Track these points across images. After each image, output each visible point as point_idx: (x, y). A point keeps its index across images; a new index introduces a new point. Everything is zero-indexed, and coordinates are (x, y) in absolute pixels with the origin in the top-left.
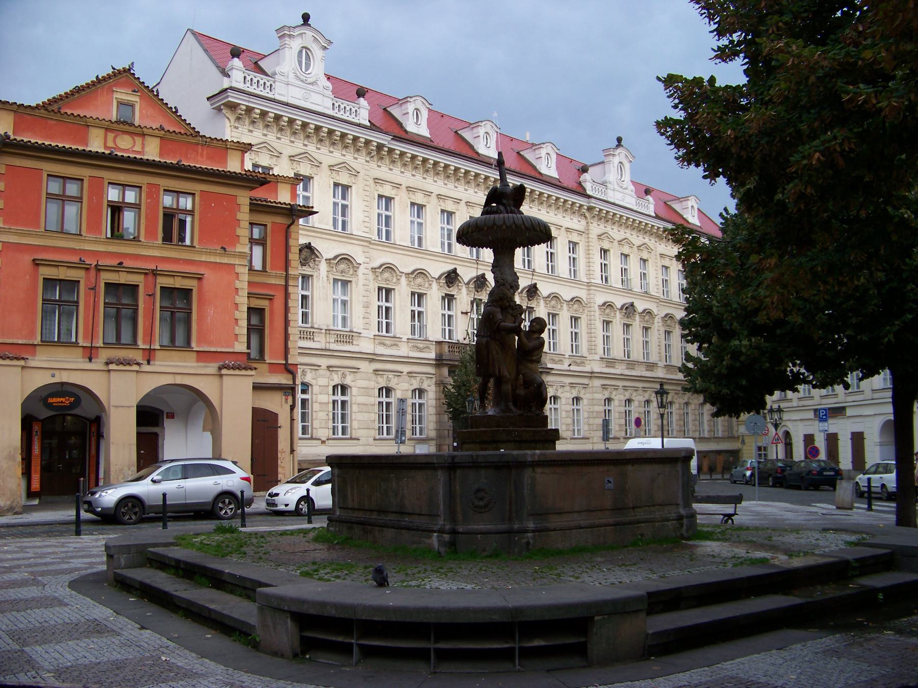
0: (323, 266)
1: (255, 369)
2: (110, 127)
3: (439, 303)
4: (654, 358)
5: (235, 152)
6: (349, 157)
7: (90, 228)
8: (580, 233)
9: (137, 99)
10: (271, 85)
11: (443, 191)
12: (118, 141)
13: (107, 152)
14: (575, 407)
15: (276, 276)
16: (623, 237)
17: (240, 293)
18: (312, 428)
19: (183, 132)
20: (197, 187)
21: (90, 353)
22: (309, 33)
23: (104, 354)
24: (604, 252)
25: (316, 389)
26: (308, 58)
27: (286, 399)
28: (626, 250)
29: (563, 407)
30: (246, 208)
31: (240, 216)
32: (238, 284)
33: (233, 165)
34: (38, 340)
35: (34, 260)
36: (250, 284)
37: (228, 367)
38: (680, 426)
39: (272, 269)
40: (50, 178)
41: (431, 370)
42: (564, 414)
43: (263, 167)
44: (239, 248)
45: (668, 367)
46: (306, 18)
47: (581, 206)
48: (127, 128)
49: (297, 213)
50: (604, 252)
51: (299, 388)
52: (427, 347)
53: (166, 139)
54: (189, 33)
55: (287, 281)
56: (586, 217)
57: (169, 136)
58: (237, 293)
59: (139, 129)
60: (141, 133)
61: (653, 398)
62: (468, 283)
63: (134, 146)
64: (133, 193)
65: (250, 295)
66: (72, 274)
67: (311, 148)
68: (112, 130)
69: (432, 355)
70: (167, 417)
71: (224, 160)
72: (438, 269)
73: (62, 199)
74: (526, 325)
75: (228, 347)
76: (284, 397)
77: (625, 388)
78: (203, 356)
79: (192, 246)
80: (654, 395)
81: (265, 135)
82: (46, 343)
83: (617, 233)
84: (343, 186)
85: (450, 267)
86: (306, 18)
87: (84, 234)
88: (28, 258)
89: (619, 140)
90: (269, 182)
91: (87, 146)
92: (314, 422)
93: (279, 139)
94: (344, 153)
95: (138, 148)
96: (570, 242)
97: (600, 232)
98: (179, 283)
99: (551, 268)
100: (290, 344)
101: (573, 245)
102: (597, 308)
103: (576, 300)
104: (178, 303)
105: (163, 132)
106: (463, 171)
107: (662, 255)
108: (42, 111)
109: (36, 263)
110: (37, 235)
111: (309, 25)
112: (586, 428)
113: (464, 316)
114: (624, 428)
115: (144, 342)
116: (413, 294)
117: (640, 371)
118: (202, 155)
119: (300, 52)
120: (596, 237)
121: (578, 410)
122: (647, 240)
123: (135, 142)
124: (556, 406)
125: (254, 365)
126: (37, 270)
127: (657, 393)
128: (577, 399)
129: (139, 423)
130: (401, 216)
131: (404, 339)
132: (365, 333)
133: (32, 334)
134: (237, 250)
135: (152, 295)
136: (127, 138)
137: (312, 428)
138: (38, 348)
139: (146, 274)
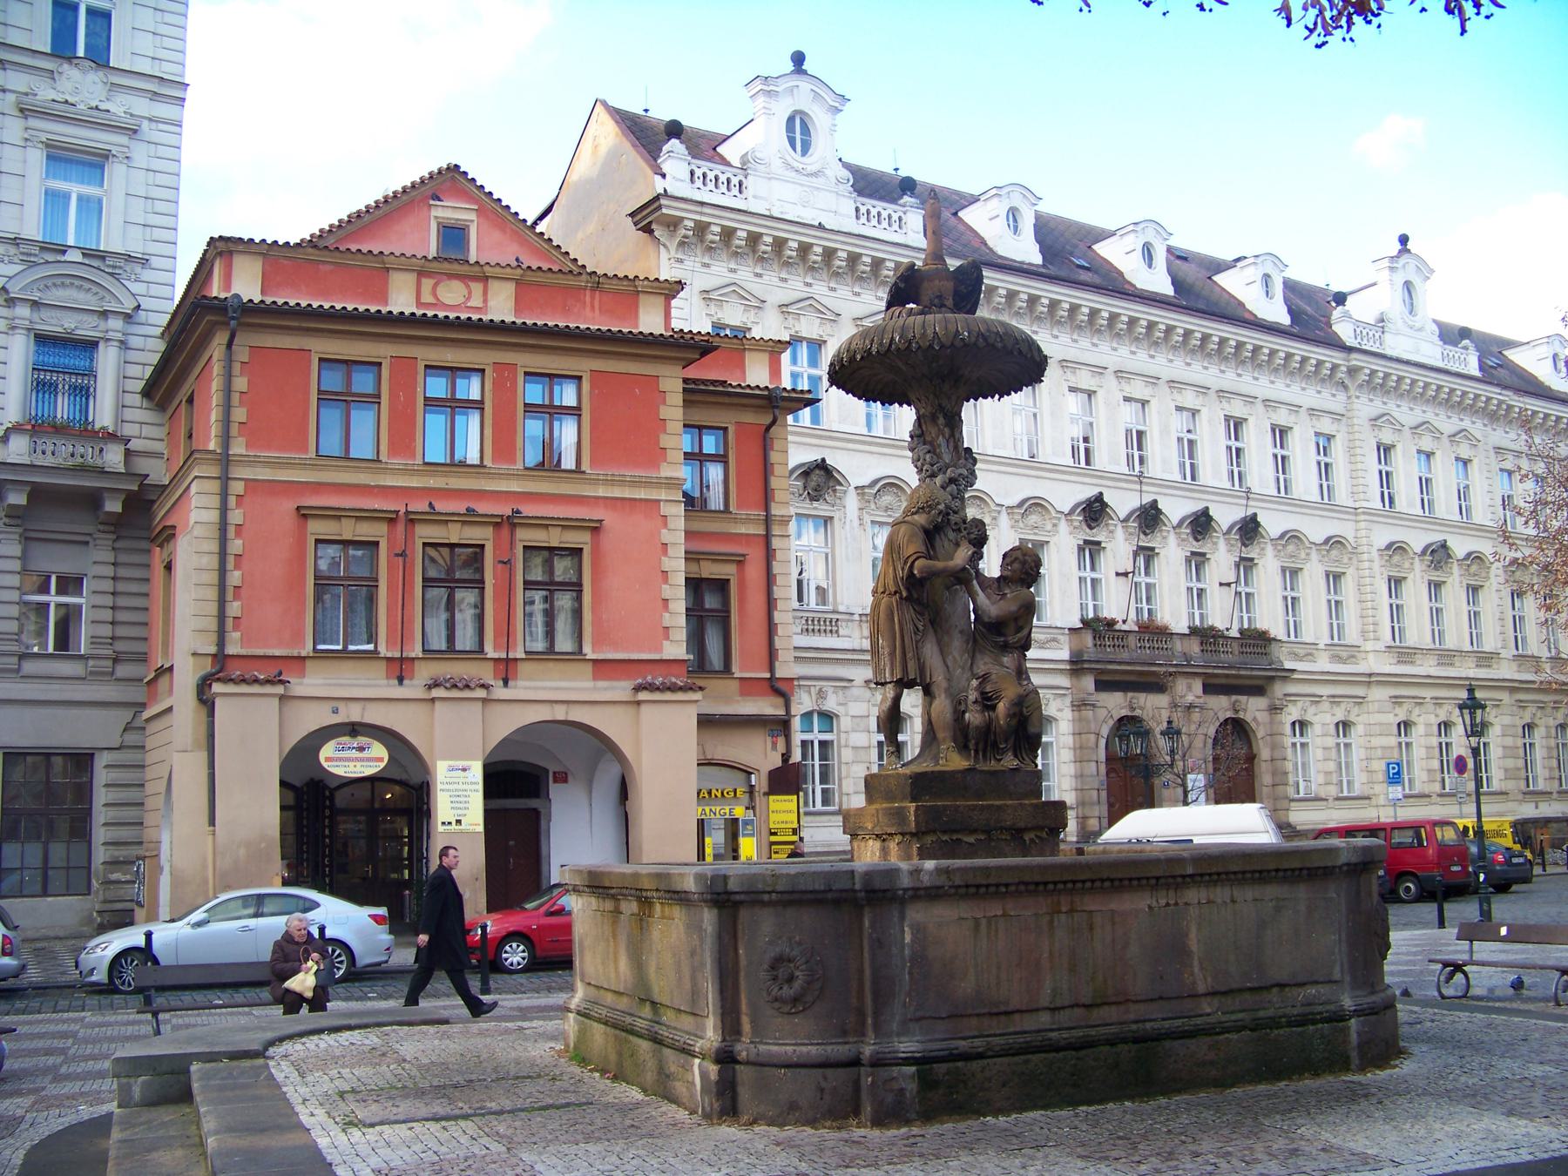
0: (852, 501)
1: (701, 689)
2: (423, 270)
3: (1278, 579)
4: (1489, 645)
5: (652, 298)
6: (745, 274)
7: (394, 450)
8: (1337, 416)
9: (473, 216)
10: (900, 219)
11: (1072, 354)
12: (441, 291)
13: (419, 312)
14: (1342, 740)
15: (748, 520)
16: (1420, 420)
17: (670, 551)
18: (841, 794)
19: (555, 268)
20: (584, 365)
21: (400, 669)
22: (804, 85)
23: (425, 672)
24: (1385, 450)
25: (845, 723)
26: (806, 130)
27: (774, 745)
28: (1387, 437)
29: (1319, 741)
30: (678, 399)
31: (665, 412)
32: (666, 536)
33: (649, 321)
34: (307, 649)
35: (298, 508)
36: (689, 534)
37: (650, 687)
38: (1551, 769)
39: (739, 507)
40: (324, 365)
41: (1064, 681)
42: (1319, 754)
43: (733, 328)
44: (666, 471)
45: (1521, 659)
46: (798, 59)
47: (1334, 367)
48: (456, 268)
49: (781, 404)
50: (1385, 450)
51: (796, 723)
52: (1054, 640)
53: (527, 284)
54: (599, 108)
55: (768, 529)
56: (1346, 388)
57: (530, 277)
58: (665, 552)
59: (477, 268)
60: (481, 275)
61: (1456, 716)
62: (1126, 520)
63: (469, 298)
64: (443, 380)
65: (691, 557)
66: (366, 531)
67: (820, 289)
68: (429, 274)
69: (1064, 654)
70: (555, 781)
71: (633, 311)
72: (1067, 495)
73: (454, 405)
74: (991, 565)
75: (650, 651)
76: (769, 740)
77: (1335, 700)
78: (603, 668)
79: (482, 466)
80: (1457, 711)
81: (808, 285)
82: (320, 656)
83: (1408, 413)
84: (810, 342)
85: (1090, 492)
86: (798, 59)
87: (383, 458)
88: (288, 505)
89: (1404, 240)
90: (716, 348)
91: (386, 304)
92: (844, 783)
93: (759, 275)
94: (1055, 332)
95: (476, 301)
96: (1317, 434)
97: (1375, 413)
98: (554, 538)
99: (1284, 486)
100: (778, 643)
101: (1324, 443)
102: (1375, 554)
103: (1333, 542)
104: (560, 574)
105: (519, 271)
106: (1106, 315)
107: (1498, 450)
108: (310, 250)
109: (303, 514)
110: (303, 465)
111: (805, 72)
112: (1364, 777)
113: (1122, 579)
114: (1556, 774)
115: (496, 647)
116: (1284, 570)
117: (1427, 667)
118: (593, 307)
119: (791, 120)
120: (1367, 425)
121: (1407, 744)
122: (1467, 423)
123: (470, 293)
124: (1304, 740)
125: (700, 683)
126: (305, 527)
127: (1461, 707)
128: (1344, 726)
129: (489, 793)
130: (1406, 470)
131: (1321, 646)
132: (1369, 646)
133: (298, 637)
134: (663, 474)
135: (508, 563)
136: (457, 285)
137: (841, 794)
138: (308, 663)
139: (497, 525)
